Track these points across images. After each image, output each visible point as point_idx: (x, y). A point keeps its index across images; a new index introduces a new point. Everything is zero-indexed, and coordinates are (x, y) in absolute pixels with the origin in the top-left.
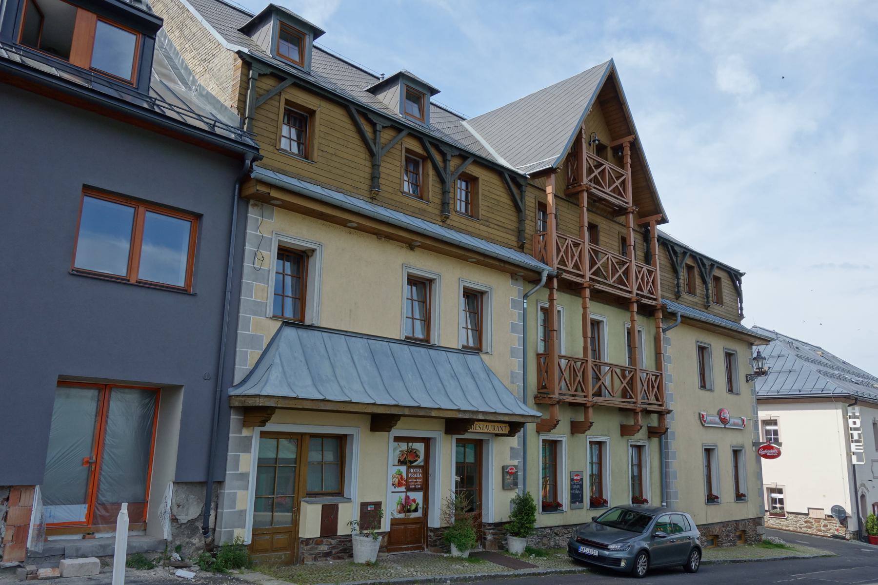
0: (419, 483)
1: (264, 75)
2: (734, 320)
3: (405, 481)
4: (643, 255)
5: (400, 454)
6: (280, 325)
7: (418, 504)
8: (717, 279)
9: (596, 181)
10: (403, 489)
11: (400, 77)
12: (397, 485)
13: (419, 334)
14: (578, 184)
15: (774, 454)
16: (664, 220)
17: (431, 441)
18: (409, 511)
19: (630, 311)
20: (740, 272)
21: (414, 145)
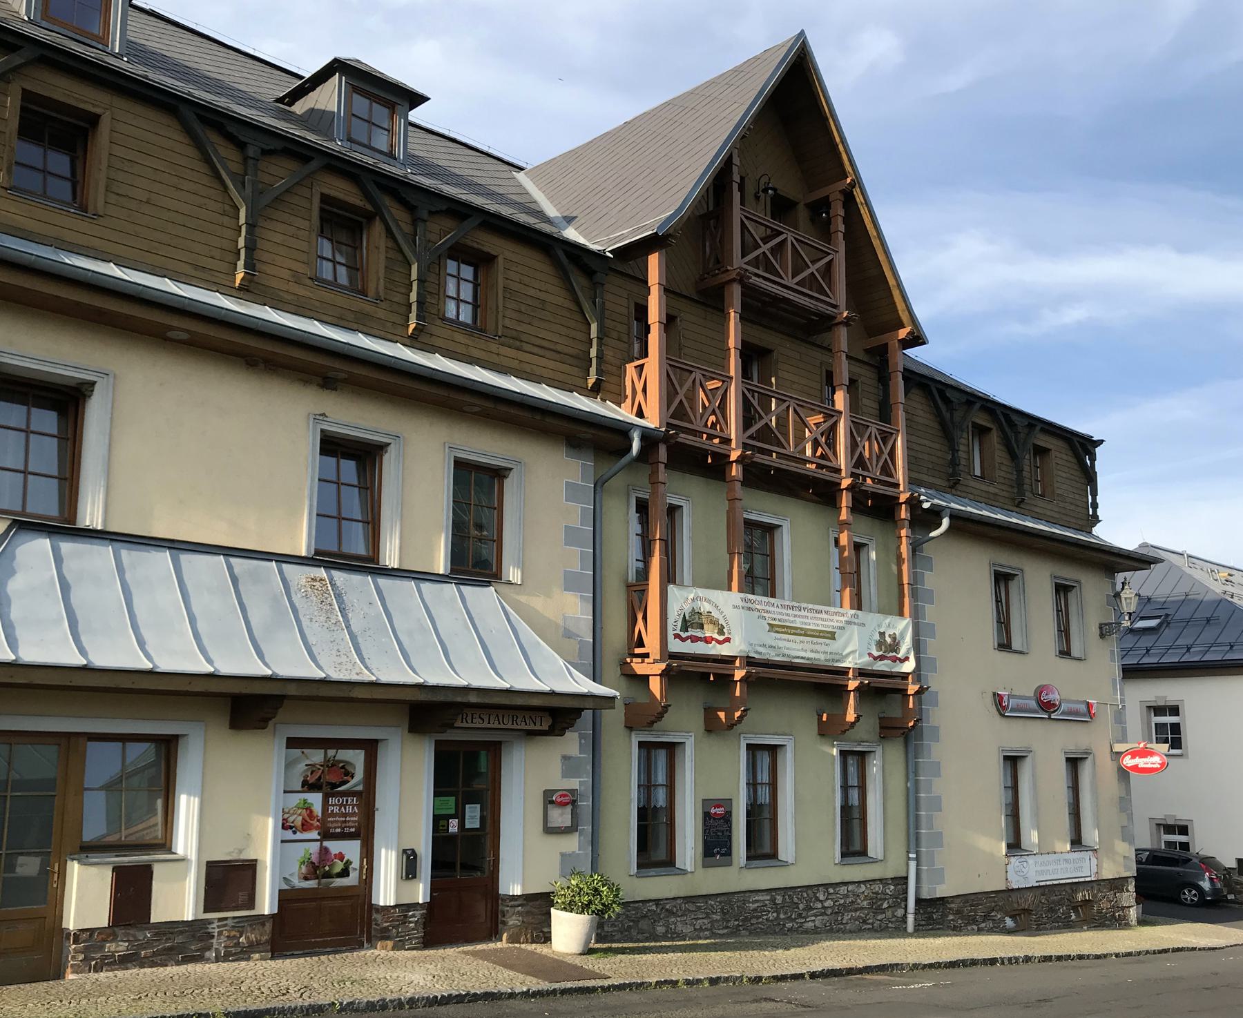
0: (351, 824)
1: (437, 212)
2: (1078, 527)
3: (318, 821)
4: (876, 406)
5: (307, 770)
6: (6, 527)
7: (348, 863)
8: (1041, 452)
9: (763, 262)
10: (314, 835)
11: (337, 67)
12: (300, 828)
13: (359, 547)
14: (722, 270)
15: (1154, 766)
16: (917, 339)
17: (778, 751)
18: (328, 875)
19: (651, 461)
20: (1094, 439)
21: (341, 189)
